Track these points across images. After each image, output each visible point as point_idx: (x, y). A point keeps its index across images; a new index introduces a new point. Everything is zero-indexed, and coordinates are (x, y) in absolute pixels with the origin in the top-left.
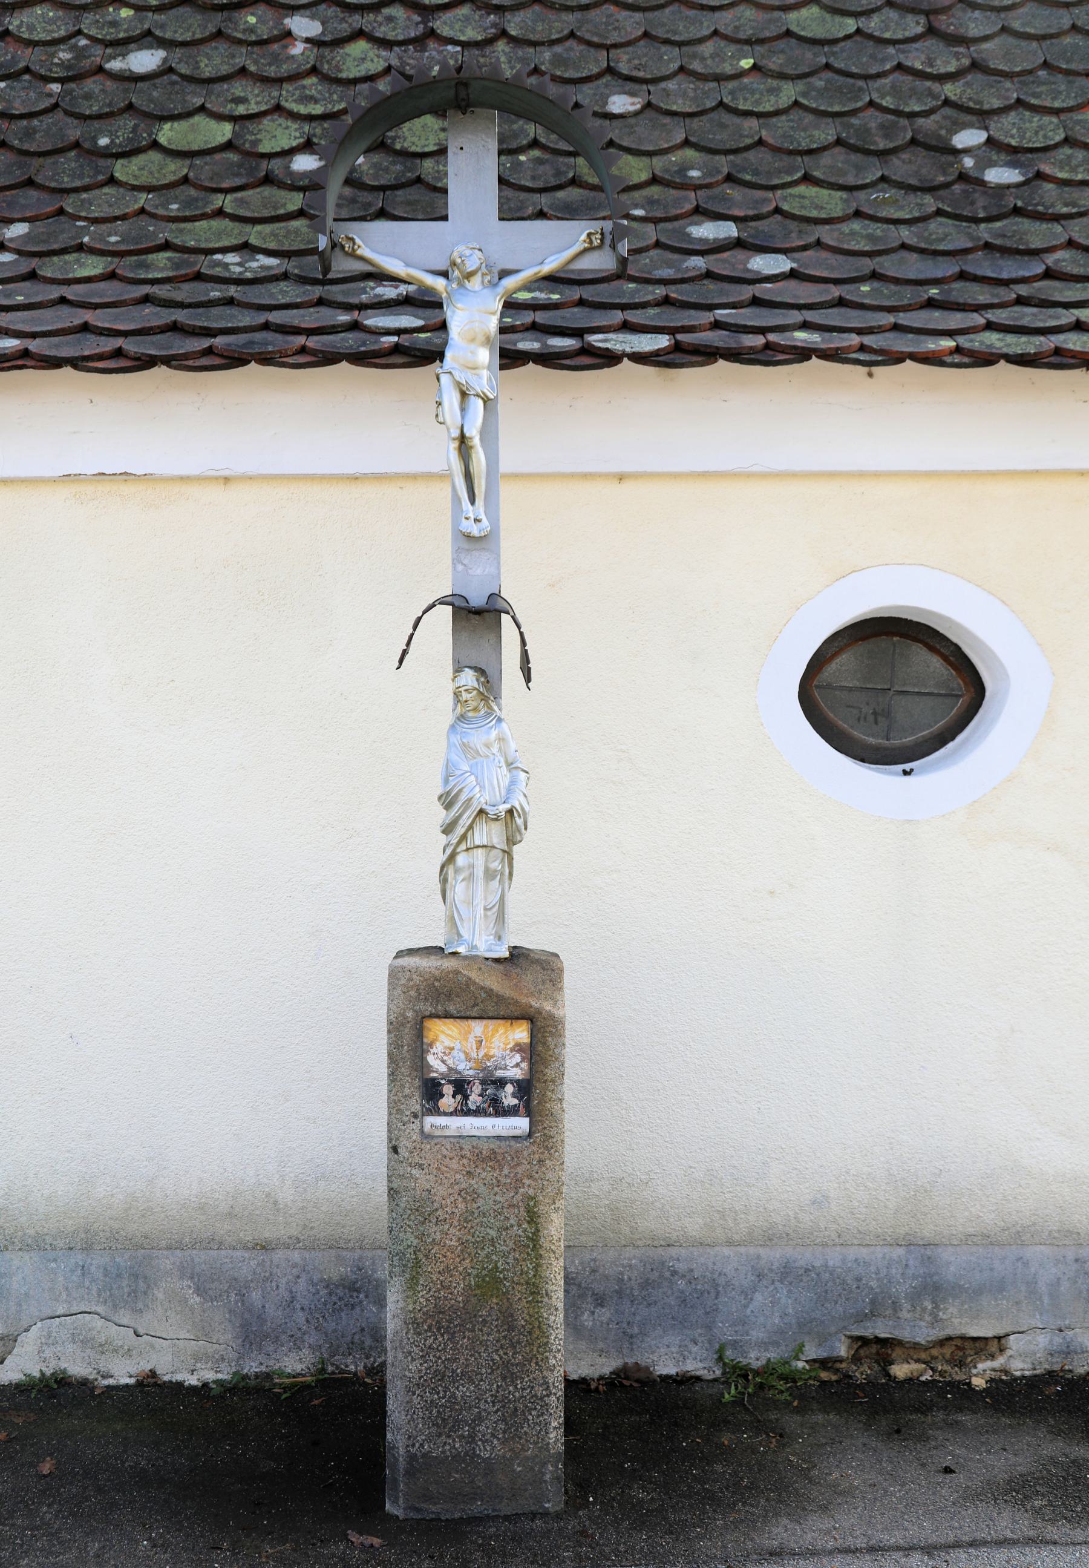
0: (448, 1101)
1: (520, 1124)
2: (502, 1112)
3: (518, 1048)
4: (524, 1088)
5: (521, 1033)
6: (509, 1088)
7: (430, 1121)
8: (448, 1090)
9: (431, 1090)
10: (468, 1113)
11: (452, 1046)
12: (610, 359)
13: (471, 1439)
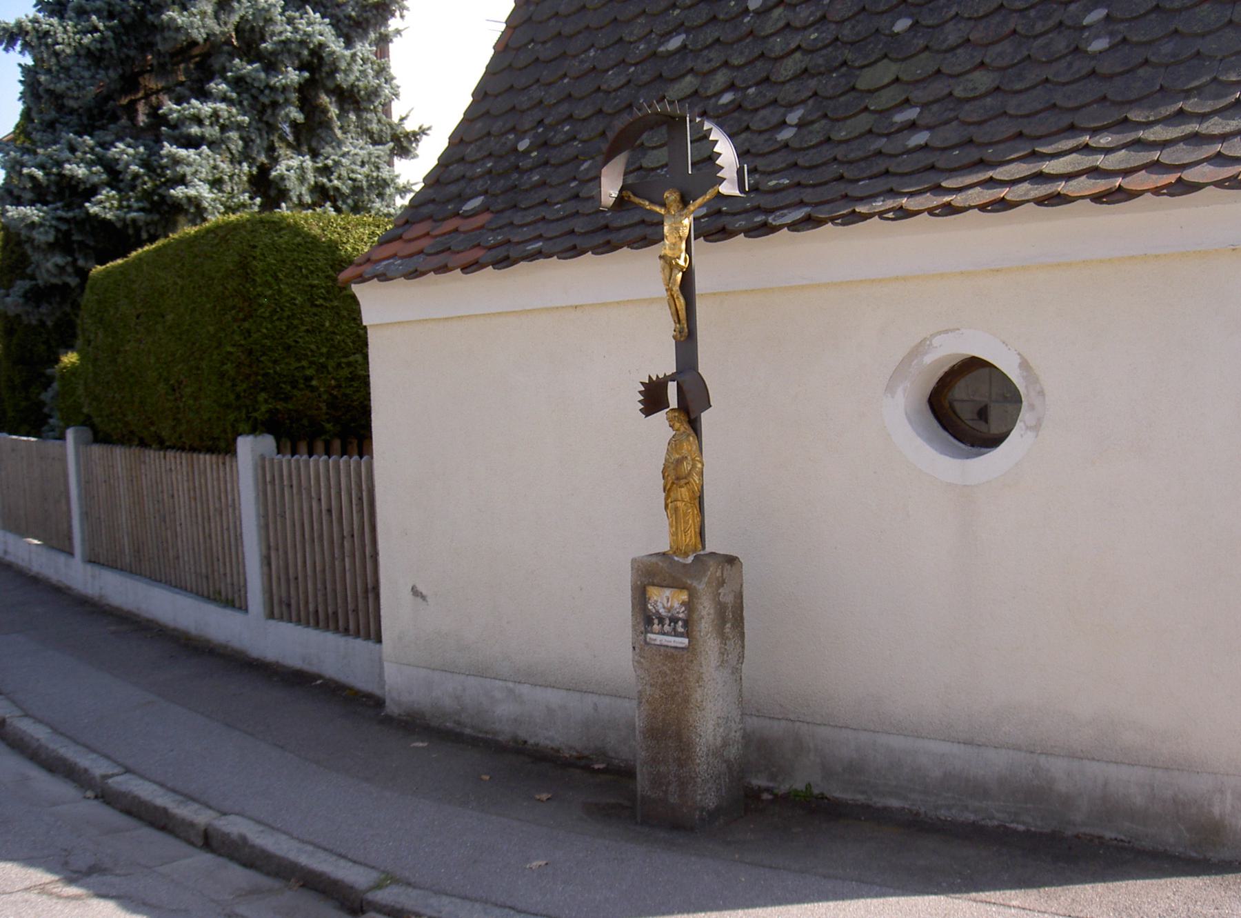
0: (656, 627)
1: (684, 642)
2: (677, 634)
3: (683, 604)
4: (686, 623)
5: (684, 596)
6: (680, 623)
7: (650, 635)
8: (656, 621)
9: (648, 621)
10: (664, 634)
11: (664, 600)
12: (1195, 187)
13: (666, 792)
